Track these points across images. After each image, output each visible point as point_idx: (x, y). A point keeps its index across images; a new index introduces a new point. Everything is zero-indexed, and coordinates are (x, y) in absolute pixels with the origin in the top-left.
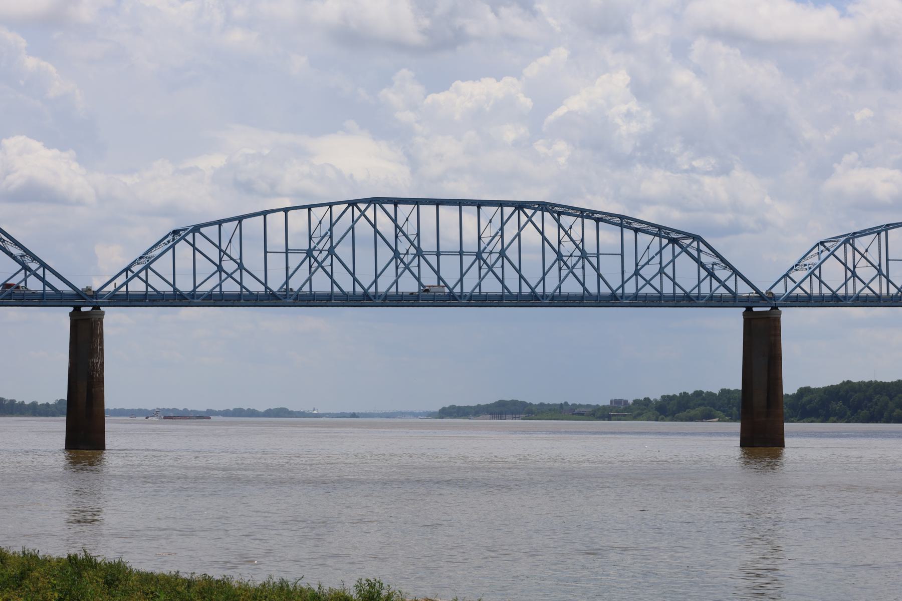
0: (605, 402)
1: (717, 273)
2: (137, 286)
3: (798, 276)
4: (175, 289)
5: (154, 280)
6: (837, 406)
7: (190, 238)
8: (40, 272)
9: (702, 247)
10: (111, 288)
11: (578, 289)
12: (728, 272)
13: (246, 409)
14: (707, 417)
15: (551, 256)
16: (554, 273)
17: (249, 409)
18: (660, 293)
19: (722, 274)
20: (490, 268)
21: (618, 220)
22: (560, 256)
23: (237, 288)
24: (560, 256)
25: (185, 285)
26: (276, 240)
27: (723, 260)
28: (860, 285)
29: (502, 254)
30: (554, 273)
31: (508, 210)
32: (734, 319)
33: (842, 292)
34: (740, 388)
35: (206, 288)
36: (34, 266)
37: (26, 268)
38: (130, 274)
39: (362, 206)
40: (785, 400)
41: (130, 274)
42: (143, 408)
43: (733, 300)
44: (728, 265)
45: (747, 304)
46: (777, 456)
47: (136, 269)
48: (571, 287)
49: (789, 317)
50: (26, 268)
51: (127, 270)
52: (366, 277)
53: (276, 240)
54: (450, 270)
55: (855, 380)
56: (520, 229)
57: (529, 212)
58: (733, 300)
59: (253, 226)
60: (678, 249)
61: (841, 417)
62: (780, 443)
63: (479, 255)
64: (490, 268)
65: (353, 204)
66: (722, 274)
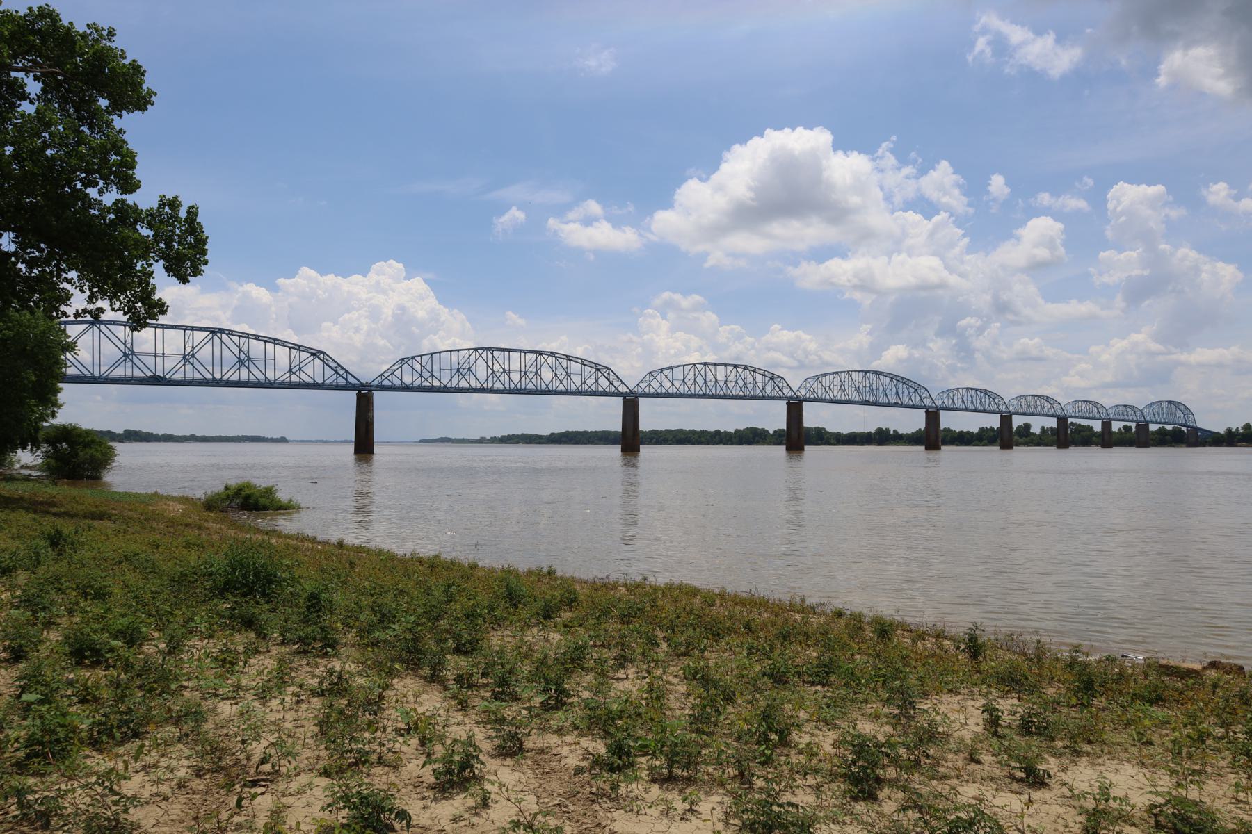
0: (1222, 430)
1: (614, 383)
2: (295, 379)
3: (643, 385)
4: (213, 377)
5: (303, 376)
6: (564, 439)
7: (410, 362)
8: (345, 376)
9: (611, 372)
10: (376, 382)
11: (467, 385)
12: (343, 371)
13: (1222, 432)
14: (518, 443)
15: (490, 371)
16: (491, 378)
17: (523, 434)
18: (92, 374)
19: (616, 383)
20: (498, 378)
21: (580, 361)
22: (493, 372)
23: (345, 382)
24: (493, 372)
25: (319, 380)
26: (446, 365)
27: (618, 378)
28: (587, 387)
29: (469, 369)
30: (490, 379)
31: (730, 368)
32: (352, 396)
33: (449, 385)
34: (620, 430)
35: (329, 381)
36: (341, 372)
37: (337, 373)
38: (383, 378)
39: (480, 351)
40: (641, 435)
41: (383, 378)
42: (965, 430)
43: (617, 394)
44: (343, 368)
45: (788, 399)
46: (637, 455)
47: (386, 375)
48: (498, 385)
49: (378, 397)
50: (337, 373)
51: (382, 375)
52: (445, 381)
53: (446, 365)
54: (516, 377)
55: (570, 430)
56: (476, 360)
57: (546, 357)
58: (617, 394)
59: (436, 356)
60: (600, 374)
61: (565, 443)
62: (638, 451)
63: (458, 370)
64: (498, 378)
65: (476, 350)
66: (616, 383)
